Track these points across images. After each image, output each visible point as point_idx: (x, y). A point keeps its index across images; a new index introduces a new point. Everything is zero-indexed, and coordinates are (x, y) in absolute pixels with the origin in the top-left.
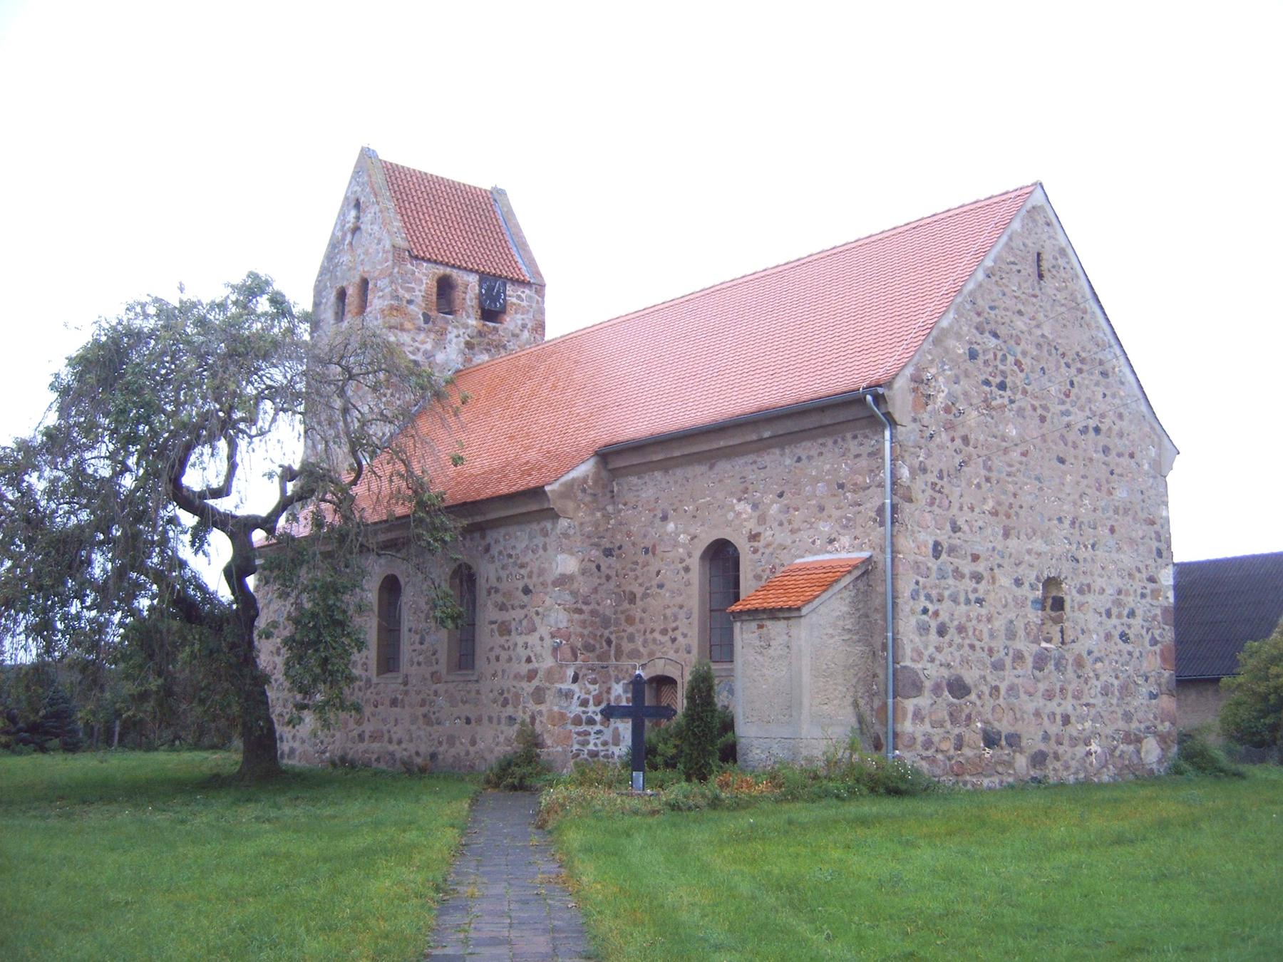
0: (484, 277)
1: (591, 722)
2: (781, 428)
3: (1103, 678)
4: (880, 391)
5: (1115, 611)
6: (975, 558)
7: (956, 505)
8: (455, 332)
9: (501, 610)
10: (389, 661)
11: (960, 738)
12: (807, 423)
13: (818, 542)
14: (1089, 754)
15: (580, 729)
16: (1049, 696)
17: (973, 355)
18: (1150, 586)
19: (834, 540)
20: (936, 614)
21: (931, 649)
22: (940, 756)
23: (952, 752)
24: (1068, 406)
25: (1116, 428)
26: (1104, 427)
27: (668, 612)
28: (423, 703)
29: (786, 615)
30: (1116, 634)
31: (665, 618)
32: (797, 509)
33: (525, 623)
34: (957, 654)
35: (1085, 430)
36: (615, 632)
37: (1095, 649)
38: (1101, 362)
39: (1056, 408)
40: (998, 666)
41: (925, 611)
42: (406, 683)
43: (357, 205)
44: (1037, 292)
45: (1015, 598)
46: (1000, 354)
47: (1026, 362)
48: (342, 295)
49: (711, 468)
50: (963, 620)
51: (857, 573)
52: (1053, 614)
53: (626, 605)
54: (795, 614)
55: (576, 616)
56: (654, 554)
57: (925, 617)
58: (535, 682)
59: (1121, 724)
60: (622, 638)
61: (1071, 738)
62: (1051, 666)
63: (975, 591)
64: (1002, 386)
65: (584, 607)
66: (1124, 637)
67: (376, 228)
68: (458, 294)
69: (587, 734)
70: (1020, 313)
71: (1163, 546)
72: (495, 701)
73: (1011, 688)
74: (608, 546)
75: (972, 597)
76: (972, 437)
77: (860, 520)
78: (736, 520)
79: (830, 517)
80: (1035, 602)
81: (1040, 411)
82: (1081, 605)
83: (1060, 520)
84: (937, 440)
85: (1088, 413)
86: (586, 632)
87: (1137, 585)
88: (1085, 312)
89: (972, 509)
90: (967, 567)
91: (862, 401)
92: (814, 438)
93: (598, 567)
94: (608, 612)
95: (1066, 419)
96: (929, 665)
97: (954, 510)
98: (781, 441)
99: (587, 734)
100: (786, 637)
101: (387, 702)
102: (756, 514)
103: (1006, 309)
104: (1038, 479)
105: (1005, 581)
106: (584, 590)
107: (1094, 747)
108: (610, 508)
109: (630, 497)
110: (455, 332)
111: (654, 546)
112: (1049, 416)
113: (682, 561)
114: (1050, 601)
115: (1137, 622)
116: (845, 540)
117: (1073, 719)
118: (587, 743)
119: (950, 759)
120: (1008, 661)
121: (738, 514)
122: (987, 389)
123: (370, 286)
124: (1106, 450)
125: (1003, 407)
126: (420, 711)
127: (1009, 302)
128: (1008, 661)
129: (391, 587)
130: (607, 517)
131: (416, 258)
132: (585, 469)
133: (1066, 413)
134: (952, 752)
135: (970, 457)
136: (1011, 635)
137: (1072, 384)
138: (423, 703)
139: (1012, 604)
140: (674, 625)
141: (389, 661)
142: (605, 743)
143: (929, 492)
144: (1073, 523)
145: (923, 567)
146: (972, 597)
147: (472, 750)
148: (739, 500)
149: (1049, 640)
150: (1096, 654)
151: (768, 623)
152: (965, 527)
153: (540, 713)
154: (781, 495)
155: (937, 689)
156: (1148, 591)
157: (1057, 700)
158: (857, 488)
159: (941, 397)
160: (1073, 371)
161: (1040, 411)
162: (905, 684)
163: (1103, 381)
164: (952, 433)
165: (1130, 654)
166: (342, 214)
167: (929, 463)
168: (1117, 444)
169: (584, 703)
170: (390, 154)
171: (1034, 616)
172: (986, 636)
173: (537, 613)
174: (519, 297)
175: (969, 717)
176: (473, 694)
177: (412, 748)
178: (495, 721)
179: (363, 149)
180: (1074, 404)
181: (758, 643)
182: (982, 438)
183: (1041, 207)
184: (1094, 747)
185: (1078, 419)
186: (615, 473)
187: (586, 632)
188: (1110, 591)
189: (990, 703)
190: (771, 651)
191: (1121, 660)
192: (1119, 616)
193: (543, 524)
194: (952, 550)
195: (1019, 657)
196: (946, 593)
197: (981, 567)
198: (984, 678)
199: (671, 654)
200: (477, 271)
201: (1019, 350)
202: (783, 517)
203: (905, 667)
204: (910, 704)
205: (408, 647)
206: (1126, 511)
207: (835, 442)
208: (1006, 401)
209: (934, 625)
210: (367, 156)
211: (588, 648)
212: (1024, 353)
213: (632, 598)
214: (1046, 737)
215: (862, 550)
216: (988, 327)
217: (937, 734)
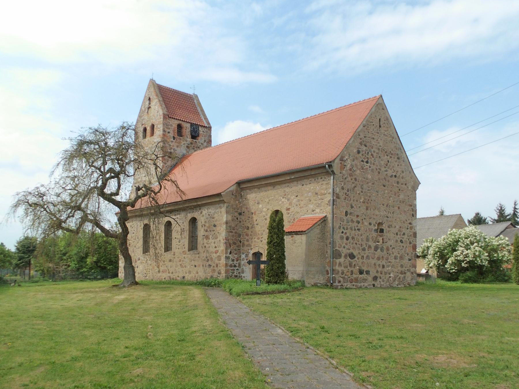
1: (235, 266)
2: (297, 175)
3: (395, 254)
4: (331, 164)
5: (399, 233)
6: (358, 216)
7: (352, 199)
8: (183, 143)
10: (168, 248)
11: (352, 271)
12: (306, 174)
14: (390, 277)
15: (232, 268)
16: (378, 259)
17: (359, 152)
18: (410, 226)
20: (346, 233)
21: (344, 244)
22: (346, 277)
23: (350, 276)
24: (387, 169)
25: (401, 176)
26: (397, 175)
28: (180, 261)
30: (399, 241)
34: (351, 246)
35: (392, 176)
37: (392, 245)
38: (397, 155)
39: (383, 169)
40: (364, 250)
41: (343, 232)
42: (174, 255)
44: (379, 132)
45: (369, 229)
46: (367, 152)
47: (375, 154)
48: (145, 130)
50: (354, 235)
51: (322, 221)
52: (380, 234)
55: (231, 234)
57: (343, 234)
58: (218, 254)
59: (400, 268)
61: (385, 272)
62: (379, 250)
63: (357, 226)
64: (367, 162)
66: (401, 241)
67: (156, 107)
68: (184, 130)
69: (234, 270)
70: (373, 138)
71: (414, 213)
73: (367, 256)
75: (356, 228)
76: (357, 178)
77: (323, 204)
78: (281, 205)
80: (375, 230)
81: (378, 170)
82: (389, 231)
83: (383, 204)
84: (347, 179)
85: (393, 171)
86: (233, 239)
87: (406, 225)
88: (393, 138)
89: (357, 201)
90: (355, 219)
91: (325, 167)
92: (308, 179)
93: (237, 219)
94: (240, 232)
95: (386, 173)
96: (344, 249)
97: (352, 201)
98: (297, 179)
99: (234, 270)
101: (168, 261)
102: (288, 202)
103: (369, 137)
104: (377, 192)
105: (366, 224)
106: (233, 225)
107: (391, 275)
108: (240, 200)
110: (183, 143)
112: (381, 172)
113: (264, 217)
114: (379, 230)
115: (406, 236)
116: (318, 210)
117: (385, 266)
118: (233, 273)
119: (349, 277)
120: (367, 248)
121: (283, 202)
122: (362, 163)
123: (155, 127)
124: (398, 183)
125: (367, 168)
126: (179, 264)
127: (370, 135)
128: (367, 248)
129: (146, 228)
130: (240, 203)
131: (170, 117)
133: (386, 171)
134: (350, 276)
135: (357, 184)
136: (368, 240)
137: (388, 161)
138: (180, 261)
139: (368, 230)
141: (168, 248)
142: (239, 273)
143: (344, 196)
144: (387, 205)
145: (342, 220)
146: (356, 228)
147: (197, 275)
149: (378, 242)
150: (393, 247)
151: (295, 236)
152: (355, 207)
154: (297, 196)
155: (345, 256)
156: (409, 227)
157: (381, 260)
159: (348, 167)
160: (389, 157)
161: (378, 170)
162: (337, 255)
163: (398, 161)
164: (351, 177)
165: (403, 247)
166: (144, 102)
167: (345, 186)
168: (401, 181)
169: (233, 260)
170: (159, 82)
171: (375, 234)
172: (360, 240)
174: (203, 131)
175: (355, 265)
177: (177, 275)
180: (389, 168)
181: (291, 242)
182: (360, 179)
183: (381, 104)
184: (391, 275)
185: (390, 173)
186: (242, 189)
187: (233, 239)
188: (397, 227)
189: (361, 261)
190: (296, 244)
191: (400, 248)
192: (400, 235)
193: (220, 205)
194: (351, 214)
195: (370, 247)
196: (349, 227)
197: (359, 219)
198: (359, 253)
199: (261, 245)
201: (372, 150)
202: (298, 203)
203: (336, 250)
204: (338, 261)
205: (174, 243)
206: (403, 202)
208: (368, 167)
209: (345, 236)
210: (152, 82)
211: (234, 243)
212: (374, 152)
214: (377, 272)
216: (363, 143)
217: (345, 270)
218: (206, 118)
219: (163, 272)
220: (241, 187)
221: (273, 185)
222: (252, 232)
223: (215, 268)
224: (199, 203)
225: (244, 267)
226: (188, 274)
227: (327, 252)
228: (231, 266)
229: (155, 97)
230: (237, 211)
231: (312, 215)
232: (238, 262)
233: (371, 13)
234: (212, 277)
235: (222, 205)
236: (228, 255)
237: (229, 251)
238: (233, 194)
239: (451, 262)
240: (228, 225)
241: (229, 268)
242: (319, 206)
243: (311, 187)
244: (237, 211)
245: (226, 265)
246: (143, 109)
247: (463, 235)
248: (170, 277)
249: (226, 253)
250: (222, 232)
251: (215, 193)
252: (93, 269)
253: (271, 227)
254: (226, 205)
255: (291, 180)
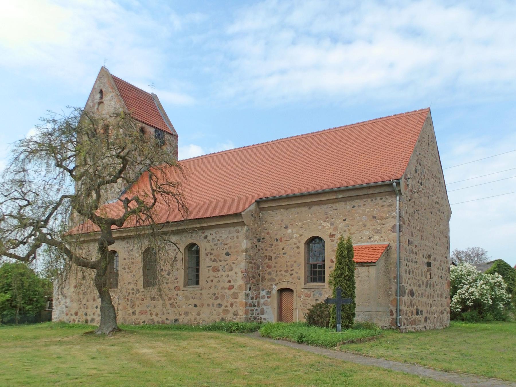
0: (157, 130)
1: (254, 306)
2: (347, 194)
9: (213, 262)
12: (360, 193)
13: (364, 238)
19: (371, 237)
27: (288, 264)
29: (368, 265)
31: (287, 266)
32: (353, 226)
33: (227, 267)
36: (262, 271)
43: (101, 92)
49: (310, 208)
53: (267, 261)
54: (374, 264)
56: (281, 241)
58: (233, 290)
60: (265, 274)
65: (252, 261)
67: (113, 103)
72: (211, 298)
74: (259, 238)
79: (369, 229)
91: (391, 185)
92: (362, 199)
93: (256, 246)
98: (345, 199)
100: (367, 273)
108: (259, 223)
109: (269, 219)
111: (281, 239)
116: (376, 238)
118: (252, 314)
121: (324, 227)
132: (253, 207)
140: (292, 269)
147: (198, 317)
148: (324, 221)
153: (236, 302)
154: (345, 220)
158: (382, 218)
162: (401, 292)
173: (234, 263)
176: (199, 295)
177: (164, 317)
178: (211, 305)
179: (102, 67)
186: (262, 209)
187: (253, 271)
193: (236, 228)
199: (290, 280)
200: (154, 127)
202: (346, 229)
207: (372, 200)
210: (104, 73)
213: (270, 258)
215: (385, 241)
218: (170, 124)
219: (141, 313)
220: (262, 206)
221: (310, 205)
222: (276, 263)
223: (229, 308)
224: (203, 225)
225: (265, 307)
226: (183, 316)
227: (390, 288)
228: (250, 306)
229: (110, 90)
230: (256, 237)
231: (368, 244)
232: (256, 301)
233: (294, 43)
234: (223, 319)
235: (240, 228)
236: (248, 292)
237: (248, 287)
238: (252, 215)
239: (456, 301)
240: (248, 253)
241: (248, 308)
242: (378, 232)
243: (365, 208)
244: (256, 237)
245: (246, 303)
246: (91, 104)
247: (464, 272)
248: (152, 320)
249: (246, 290)
250: (241, 264)
251: (232, 213)
252: (5, 310)
253: (341, 256)
254: (245, 228)
255: (336, 200)
